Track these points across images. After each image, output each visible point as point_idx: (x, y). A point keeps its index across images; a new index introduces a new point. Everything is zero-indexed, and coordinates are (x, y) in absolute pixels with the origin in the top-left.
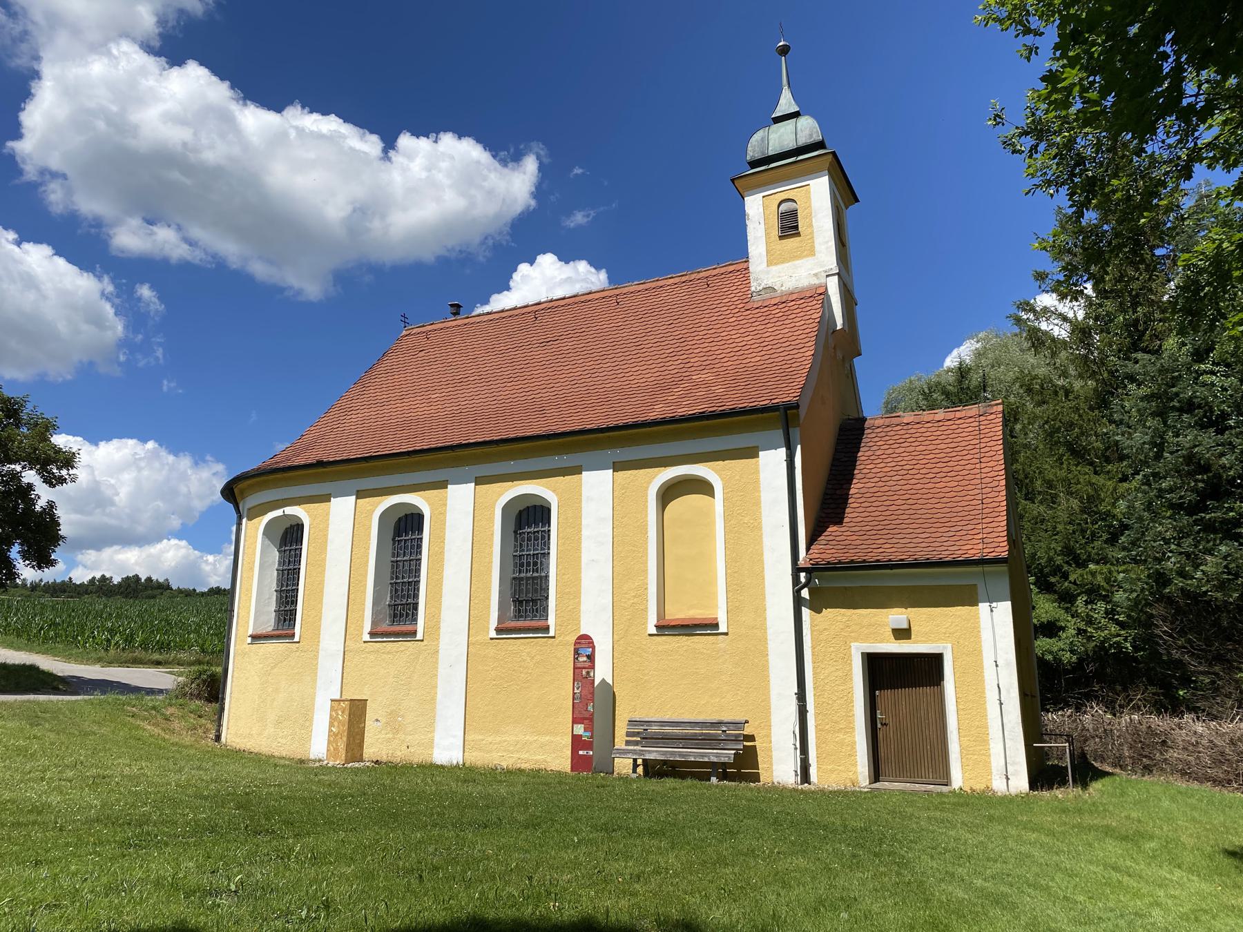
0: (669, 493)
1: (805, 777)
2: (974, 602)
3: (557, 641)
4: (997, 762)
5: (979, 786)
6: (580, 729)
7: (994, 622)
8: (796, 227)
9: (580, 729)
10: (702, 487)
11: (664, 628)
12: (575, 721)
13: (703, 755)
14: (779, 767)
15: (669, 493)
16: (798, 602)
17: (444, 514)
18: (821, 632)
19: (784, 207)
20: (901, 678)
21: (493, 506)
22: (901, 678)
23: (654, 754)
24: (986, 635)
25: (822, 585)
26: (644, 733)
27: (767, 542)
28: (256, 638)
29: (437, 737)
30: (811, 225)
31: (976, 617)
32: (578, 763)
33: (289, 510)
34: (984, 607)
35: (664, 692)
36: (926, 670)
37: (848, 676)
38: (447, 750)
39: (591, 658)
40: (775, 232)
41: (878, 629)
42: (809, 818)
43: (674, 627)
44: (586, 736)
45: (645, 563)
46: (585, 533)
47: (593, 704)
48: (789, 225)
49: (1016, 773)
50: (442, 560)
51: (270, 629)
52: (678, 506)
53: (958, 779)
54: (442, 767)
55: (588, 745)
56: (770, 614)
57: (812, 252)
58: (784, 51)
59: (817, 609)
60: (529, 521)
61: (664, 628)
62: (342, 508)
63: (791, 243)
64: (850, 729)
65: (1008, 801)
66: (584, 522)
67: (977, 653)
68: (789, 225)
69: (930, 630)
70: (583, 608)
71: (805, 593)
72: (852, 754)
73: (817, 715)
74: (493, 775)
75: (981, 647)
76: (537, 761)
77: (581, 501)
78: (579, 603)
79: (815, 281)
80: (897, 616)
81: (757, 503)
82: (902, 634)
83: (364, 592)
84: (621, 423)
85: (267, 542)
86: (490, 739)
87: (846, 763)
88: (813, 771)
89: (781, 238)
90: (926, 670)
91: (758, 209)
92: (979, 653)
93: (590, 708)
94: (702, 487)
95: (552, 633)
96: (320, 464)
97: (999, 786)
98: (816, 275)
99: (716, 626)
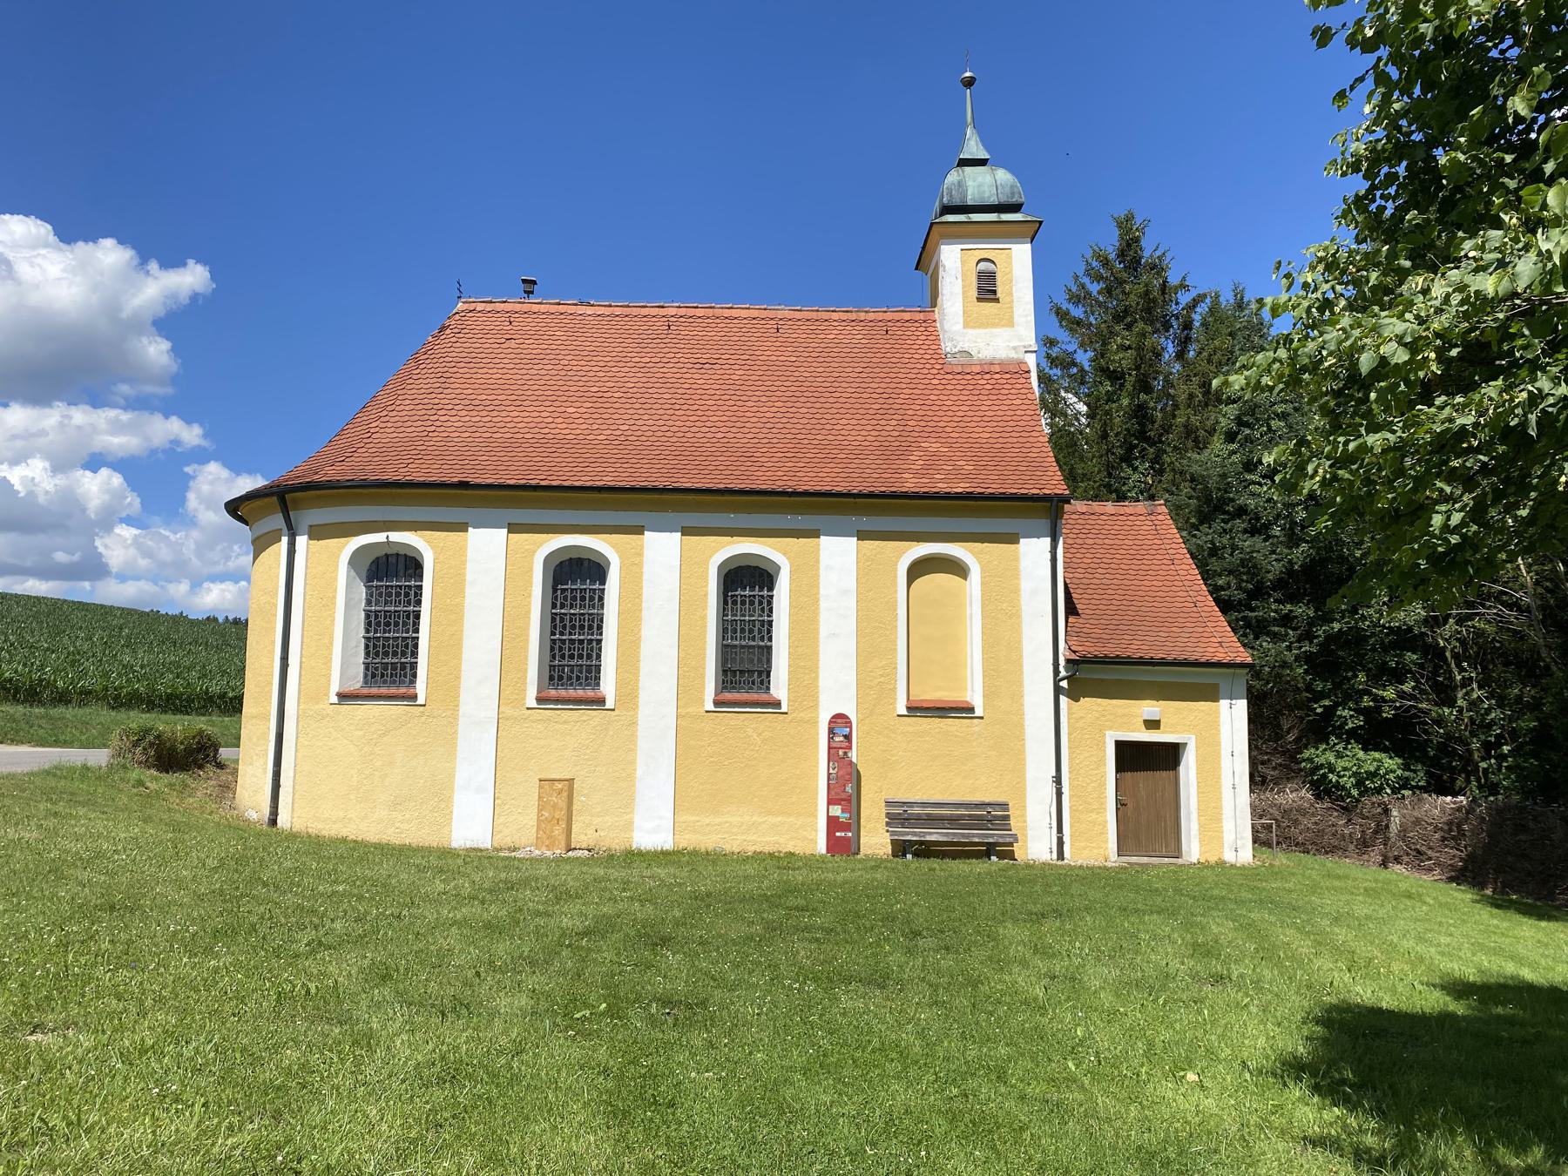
0: (918, 569)
1: (1061, 856)
2: (1216, 700)
3: (788, 717)
4: (1229, 837)
5: (1213, 859)
6: (836, 811)
7: (1233, 716)
8: (994, 292)
9: (836, 811)
10: (957, 568)
11: (914, 710)
12: (830, 802)
13: (968, 836)
14: (1036, 846)
15: (918, 569)
16: (1058, 691)
17: (640, 565)
18: (1078, 720)
19: (983, 266)
20: (1147, 761)
21: (706, 562)
22: (1147, 761)
23: (911, 834)
24: (1225, 729)
25: (1084, 675)
26: (899, 816)
27: (1027, 631)
28: (344, 697)
29: (638, 821)
30: (1011, 294)
31: (1217, 712)
32: (834, 845)
33: (397, 537)
34: (1224, 703)
35: (916, 771)
36: (1166, 757)
37: (1102, 762)
38: (653, 828)
39: (848, 737)
40: (974, 293)
41: (1130, 719)
42: (1061, 892)
43: (928, 709)
44: (844, 817)
45: (894, 642)
46: (823, 604)
47: (846, 787)
48: (987, 288)
49: (1243, 846)
50: (639, 619)
51: (358, 685)
52: (925, 582)
53: (1193, 850)
54: (648, 852)
55: (846, 827)
56: (1028, 700)
57: (1010, 323)
58: (969, 83)
59: (1074, 696)
60: (746, 585)
61: (914, 710)
62: (486, 546)
63: (988, 307)
64: (1102, 809)
65: (1093, 876)
66: (822, 592)
67: (1217, 744)
68: (987, 288)
69: (1175, 721)
70: (821, 683)
71: (1064, 684)
72: (1104, 833)
73: (1071, 797)
74: (713, 858)
75: (1216, 738)
76: (768, 843)
77: (818, 569)
78: (816, 678)
79: (1013, 355)
80: (1149, 708)
81: (1016, 590)
82: (1153, 724)
83: (525, 649)
84: (877, 490)
85: (353, 573)
86: (707, 821)
87: (1097, 842)
88: (1067, 848)
89: (979, 300)
90: (1166, 757)
91: (954, 260)
92: (1218, 744)
93: (848, 789)
94: (957, 568)
95: (784, 709)
96: (463, 485)
97: (1229, 857)
98: (1014, 348)
99: (972, 710)
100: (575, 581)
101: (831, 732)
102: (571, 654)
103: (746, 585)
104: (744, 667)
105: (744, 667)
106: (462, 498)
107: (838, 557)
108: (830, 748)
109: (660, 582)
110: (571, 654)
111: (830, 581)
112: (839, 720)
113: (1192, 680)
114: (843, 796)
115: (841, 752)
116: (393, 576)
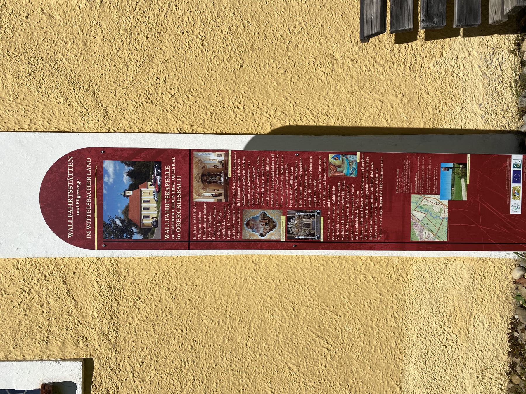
3: (101, 352)
6: (429, 213)
9: (429, 213)
12: (399, 237)
25: (148, 188)
39: (143, 165)
44: (454, 184)
100: (144, 209)
101: (121, 234)
102: (148, 209)
103: (144, 201)
104: (148, 201)
105: (148, 201)
106: (140, 214)
107: (142, 197)
108: (188, 243)
109: (144, 205)
110: (148, 209)
111: (144, 198)
112: (69, 197)
113: (148, 184)
114: (376, 181)
115: (205, 196)
116: (144, 217)
